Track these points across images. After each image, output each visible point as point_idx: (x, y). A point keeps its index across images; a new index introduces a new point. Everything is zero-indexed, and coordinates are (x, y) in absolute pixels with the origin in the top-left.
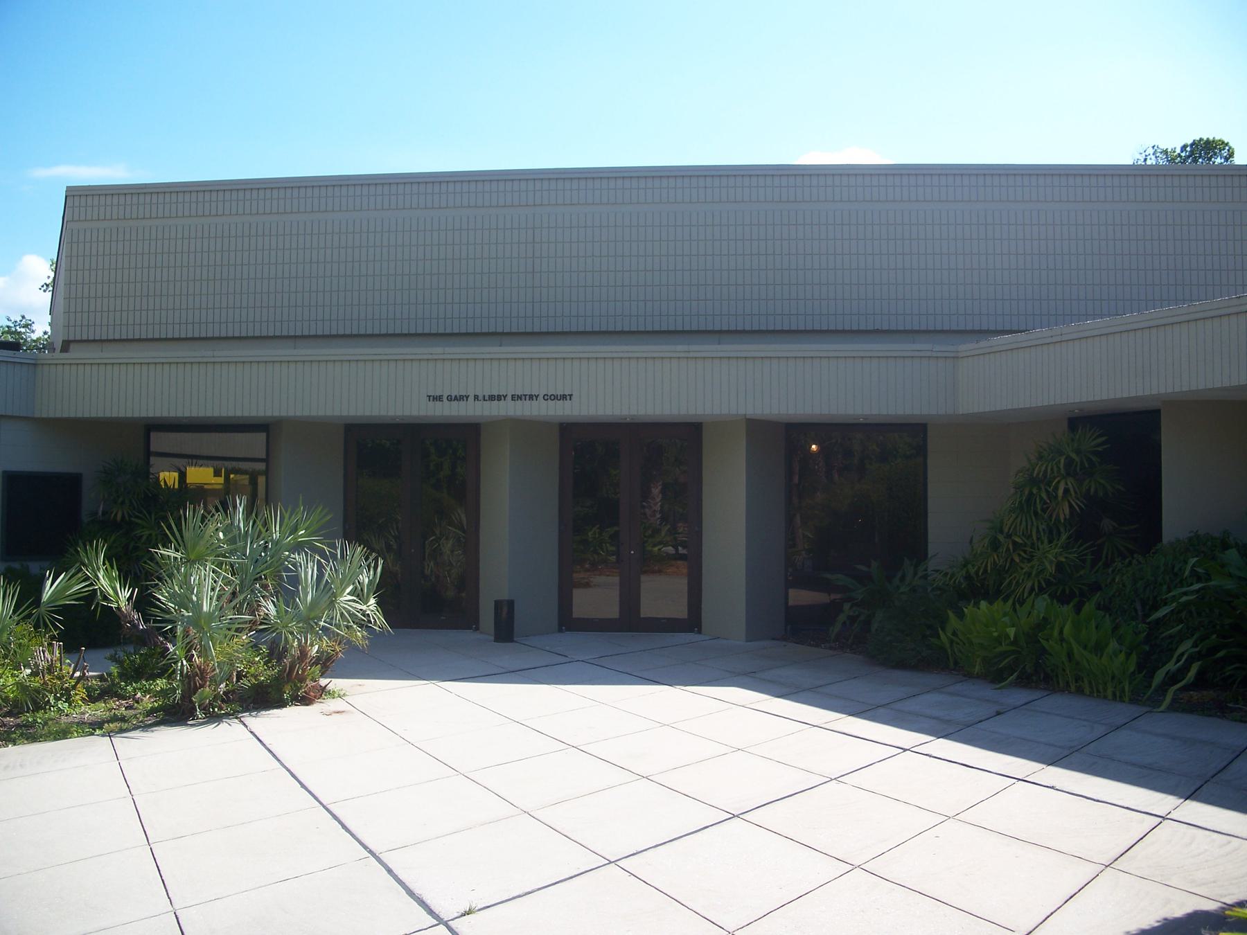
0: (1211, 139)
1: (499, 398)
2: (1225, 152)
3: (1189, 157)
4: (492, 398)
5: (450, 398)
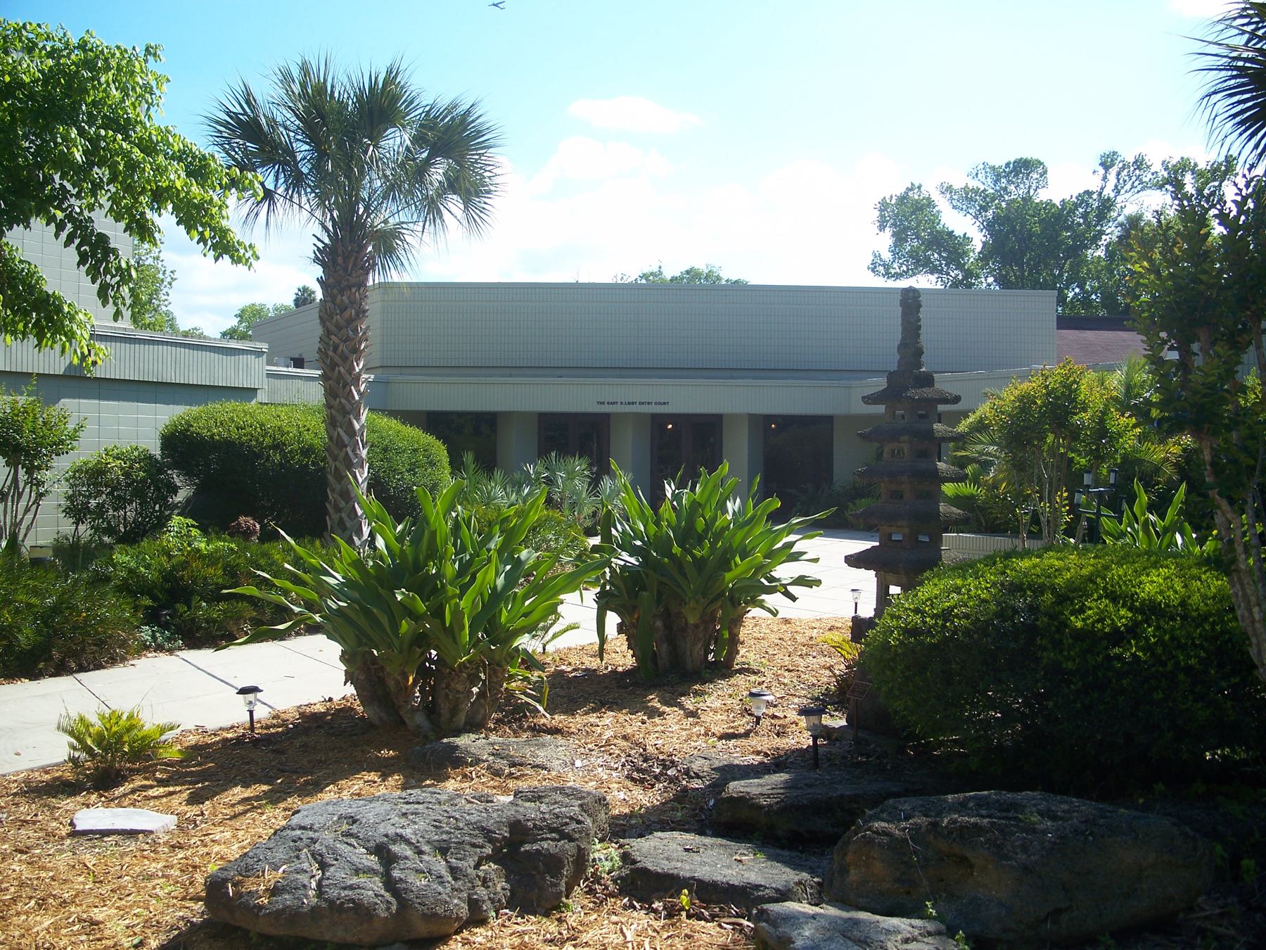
0: (1029, 158)
1: (633, 403)
2: (1040, 170)
3: (1011, 172)
4: (629, 403)
5: (608, 403)
